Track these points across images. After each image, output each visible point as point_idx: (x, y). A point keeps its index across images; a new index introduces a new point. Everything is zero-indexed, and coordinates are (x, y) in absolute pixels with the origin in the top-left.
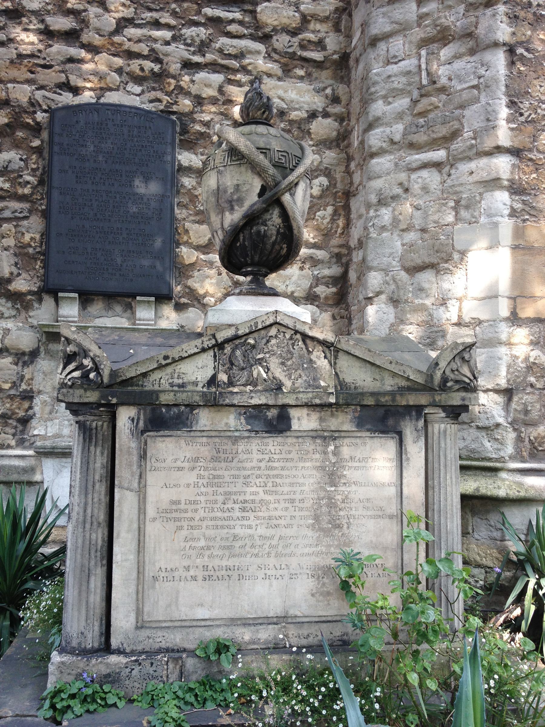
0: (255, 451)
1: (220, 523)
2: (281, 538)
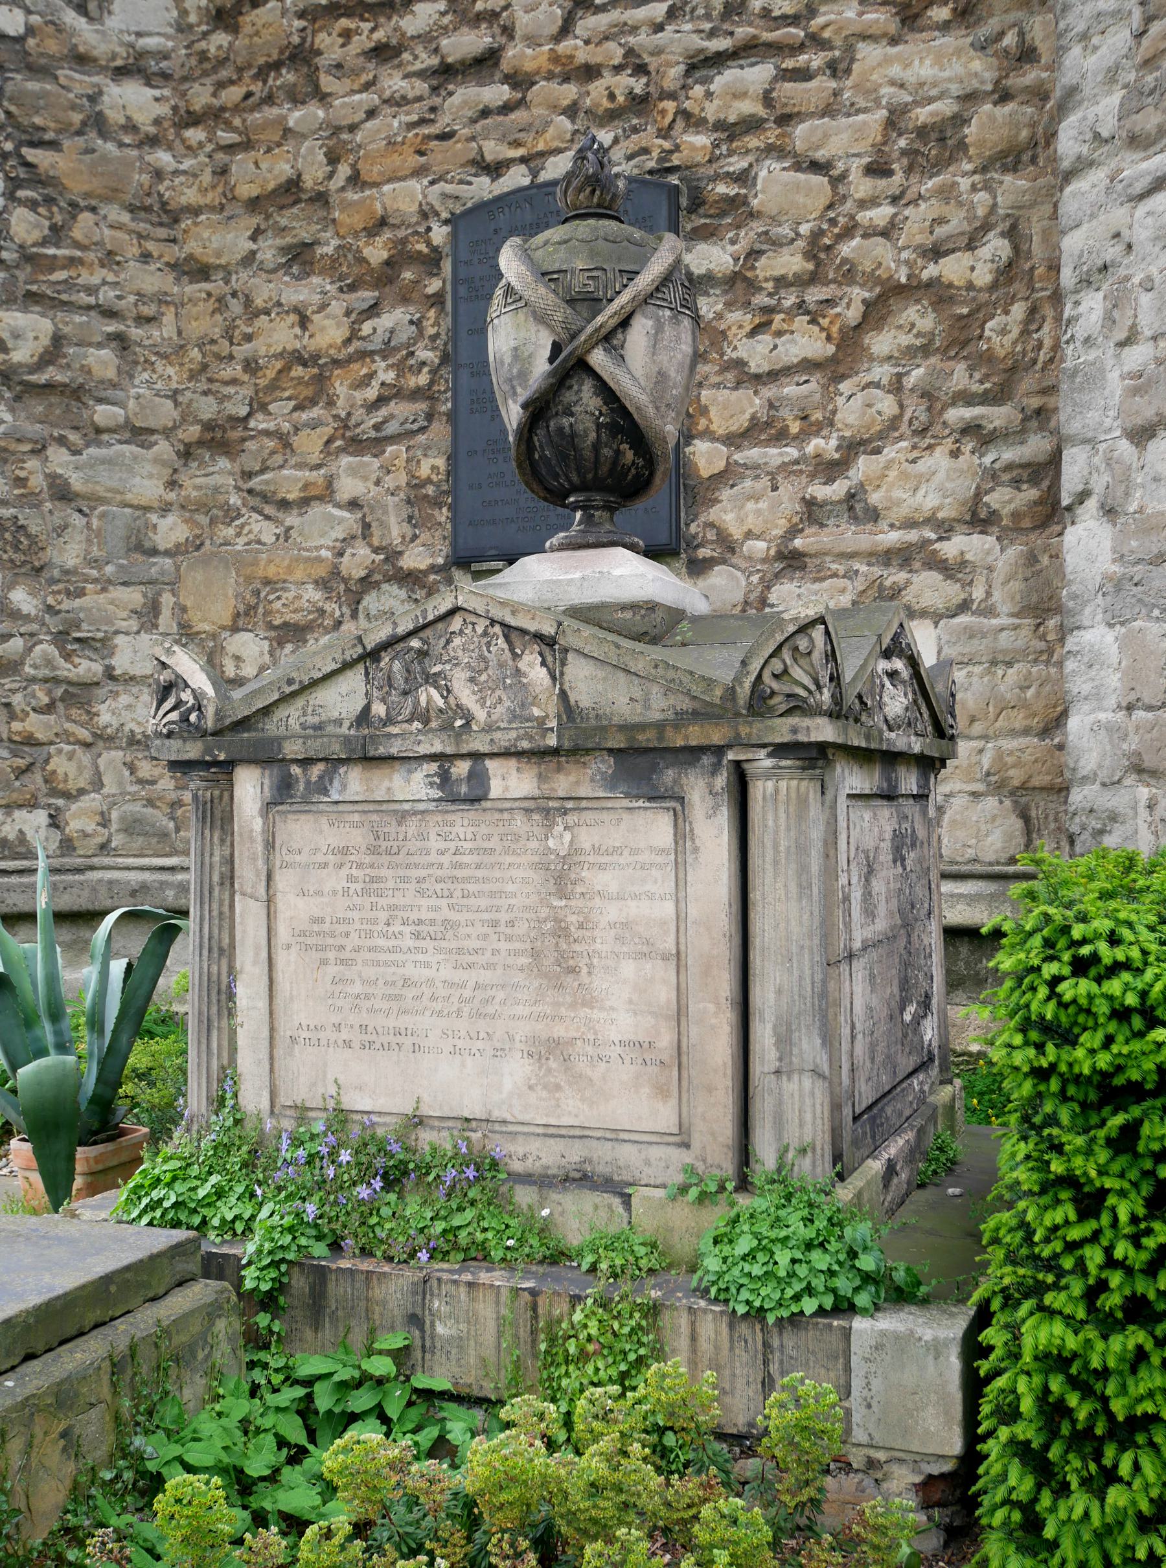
0: (433, 836)
1: (383, 957)
2: (477, 986)
